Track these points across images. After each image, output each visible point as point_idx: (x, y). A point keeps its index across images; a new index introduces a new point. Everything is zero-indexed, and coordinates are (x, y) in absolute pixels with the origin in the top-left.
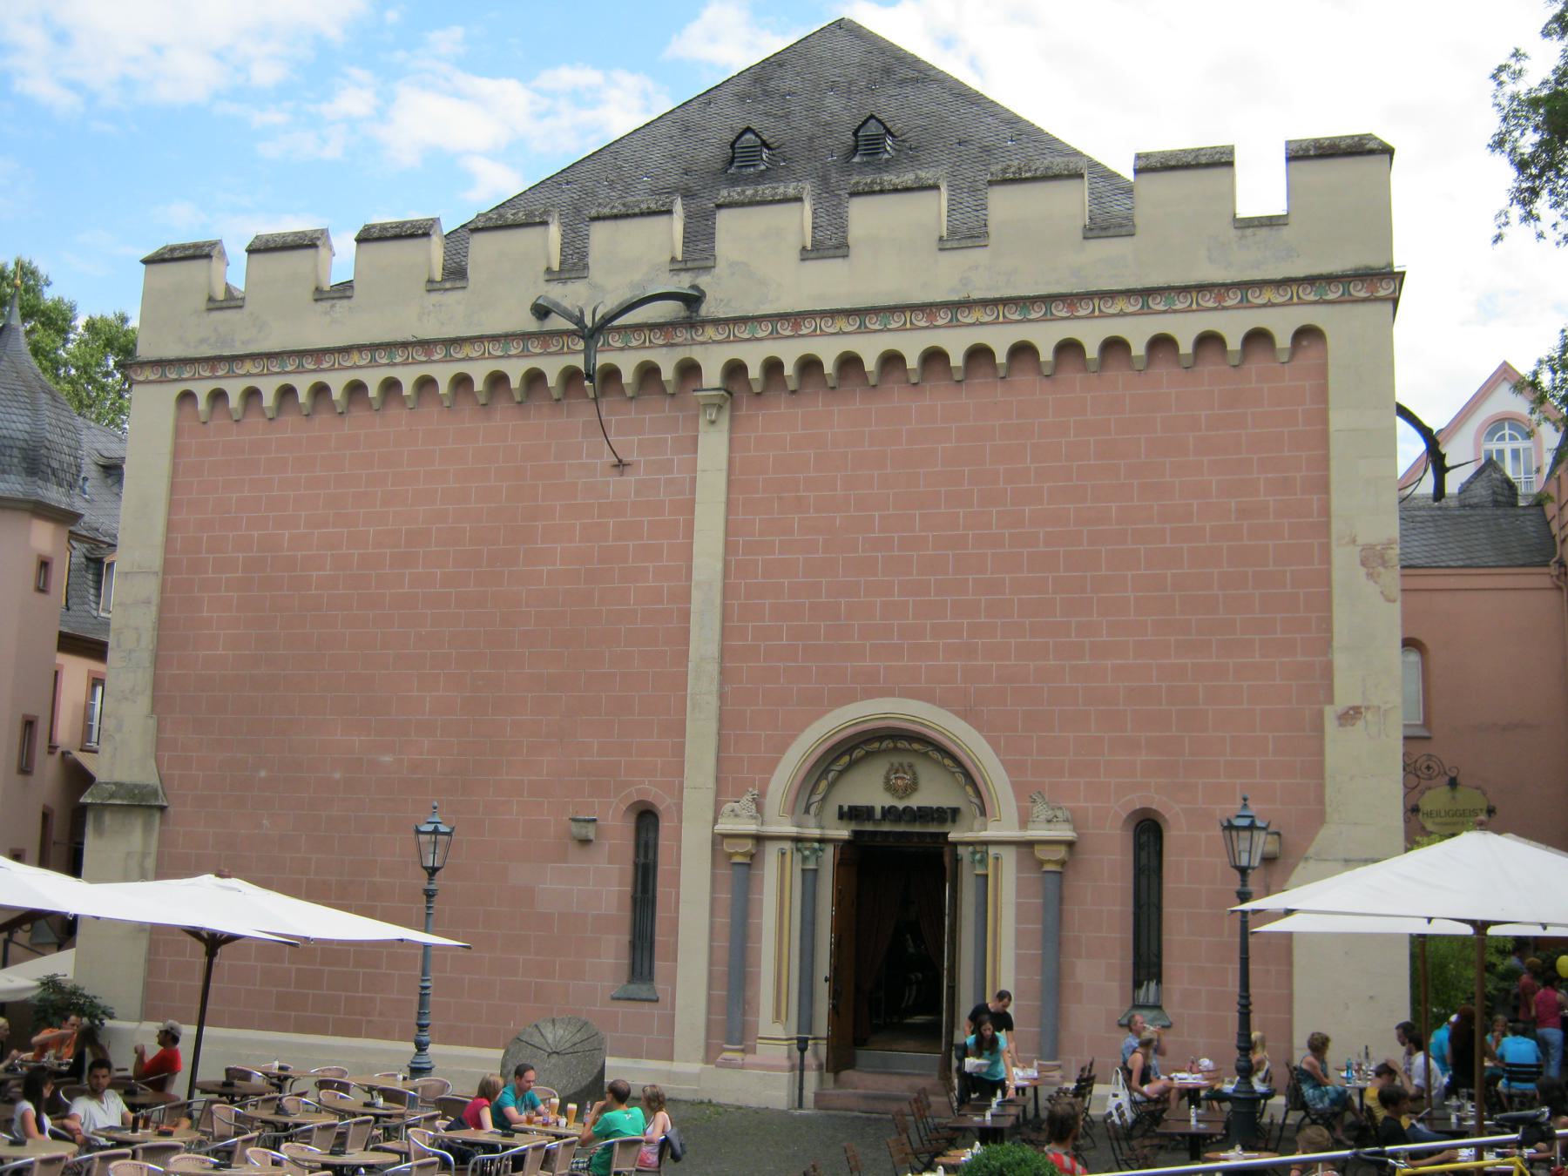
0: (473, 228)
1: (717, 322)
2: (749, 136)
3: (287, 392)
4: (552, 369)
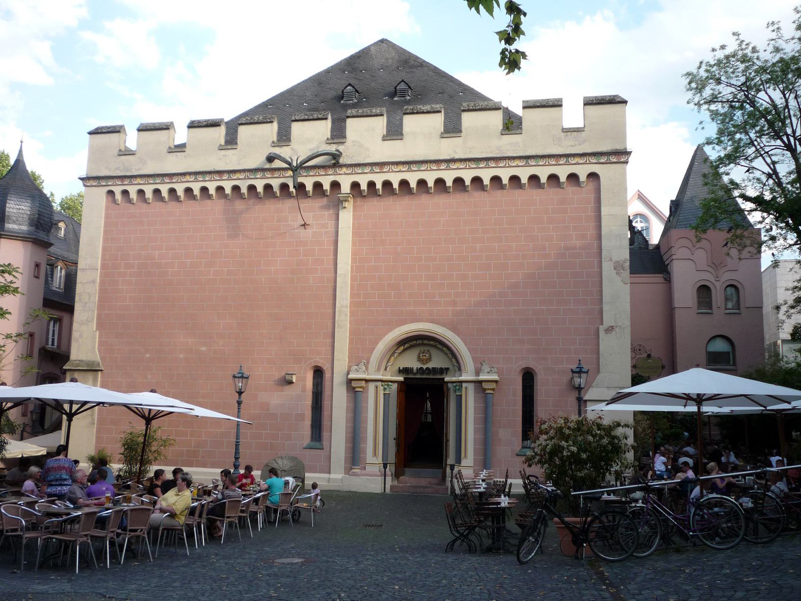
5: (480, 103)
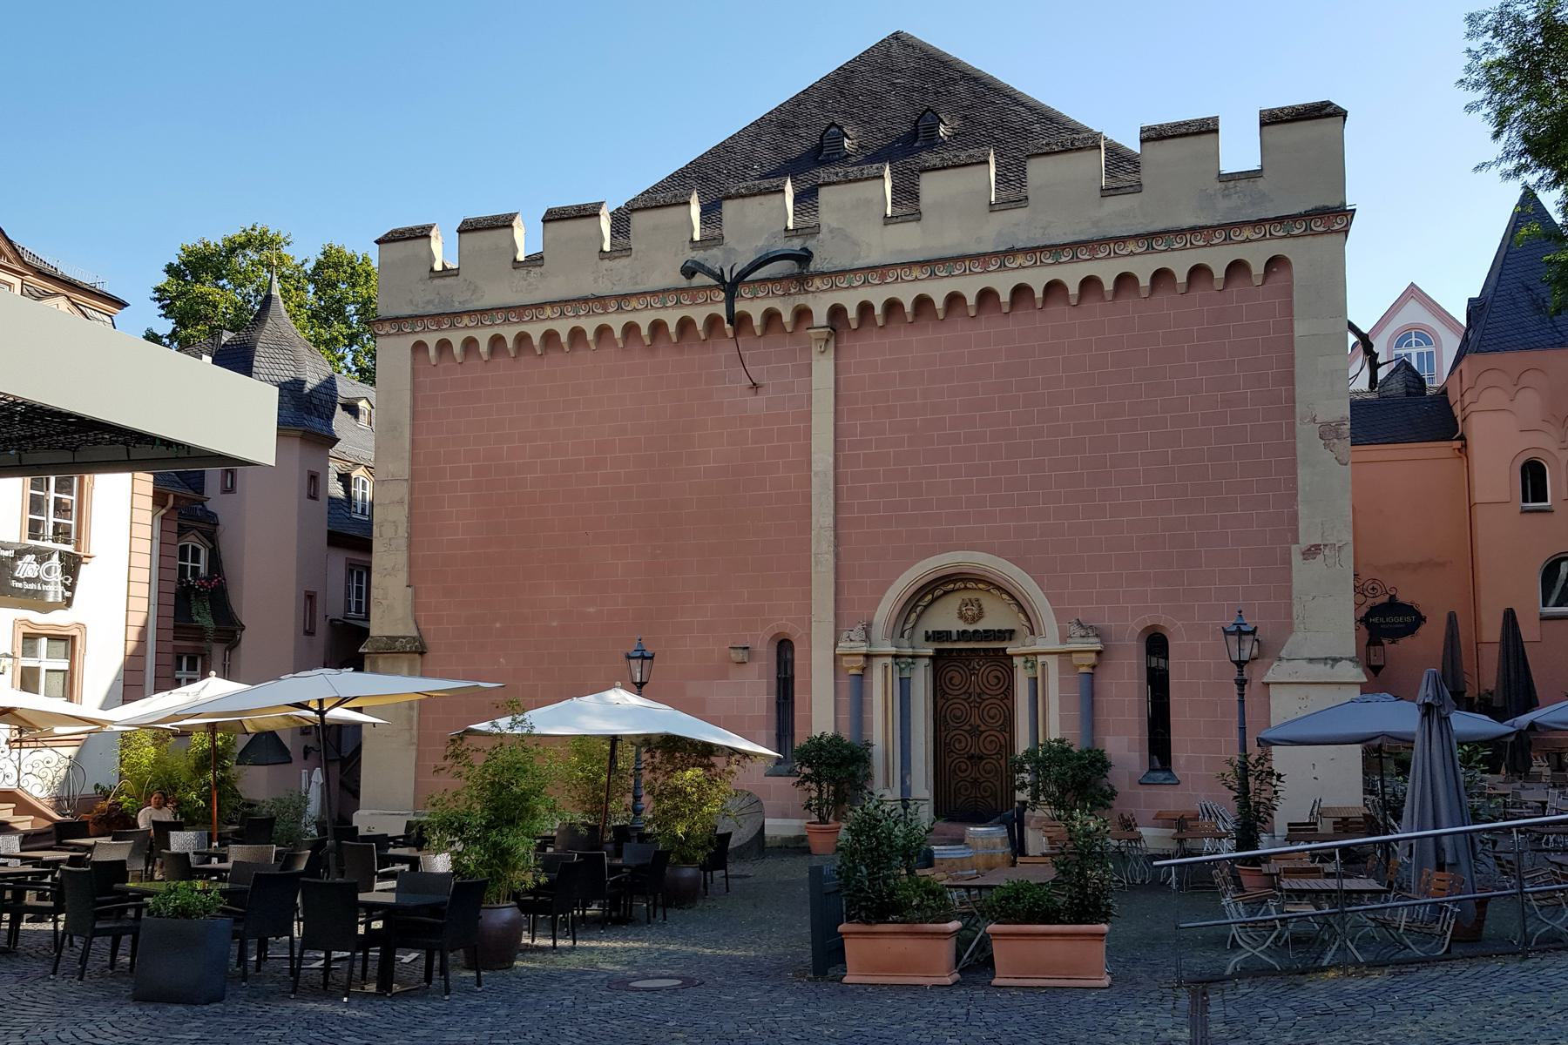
0: (633, 208)
1: (822, 274)
2: (833, 129)
3: (497, 341)
4: (699, 315)
5: (1071, 139)
